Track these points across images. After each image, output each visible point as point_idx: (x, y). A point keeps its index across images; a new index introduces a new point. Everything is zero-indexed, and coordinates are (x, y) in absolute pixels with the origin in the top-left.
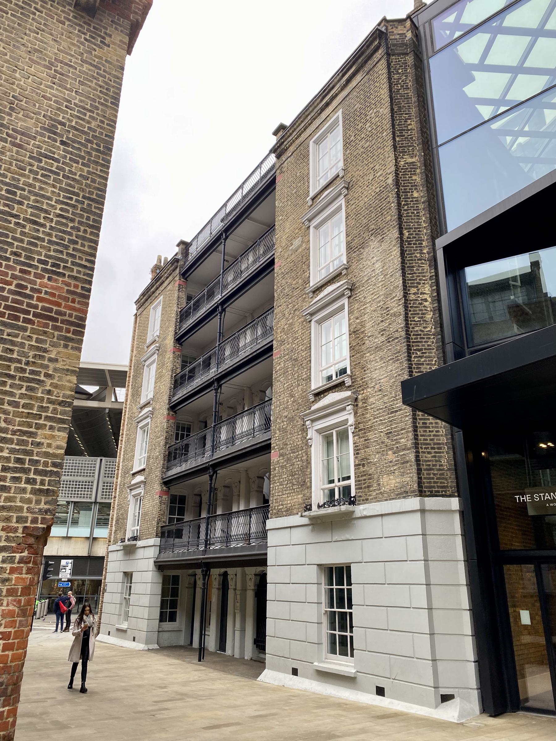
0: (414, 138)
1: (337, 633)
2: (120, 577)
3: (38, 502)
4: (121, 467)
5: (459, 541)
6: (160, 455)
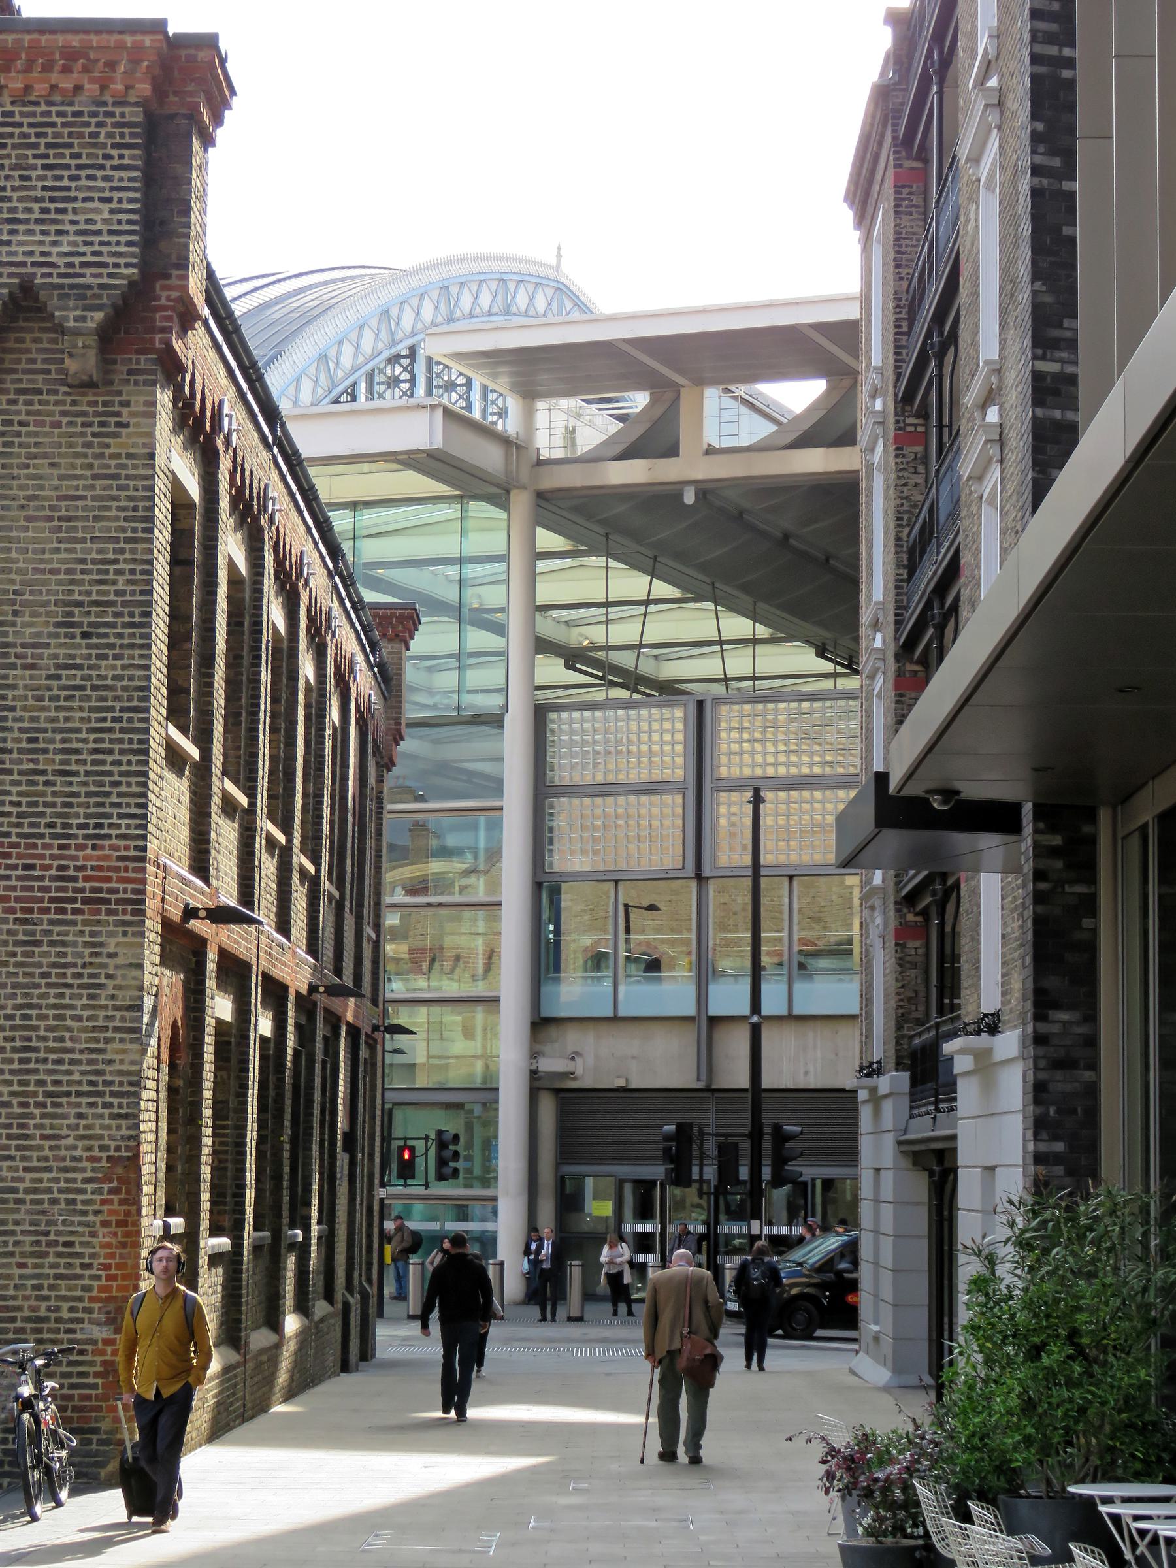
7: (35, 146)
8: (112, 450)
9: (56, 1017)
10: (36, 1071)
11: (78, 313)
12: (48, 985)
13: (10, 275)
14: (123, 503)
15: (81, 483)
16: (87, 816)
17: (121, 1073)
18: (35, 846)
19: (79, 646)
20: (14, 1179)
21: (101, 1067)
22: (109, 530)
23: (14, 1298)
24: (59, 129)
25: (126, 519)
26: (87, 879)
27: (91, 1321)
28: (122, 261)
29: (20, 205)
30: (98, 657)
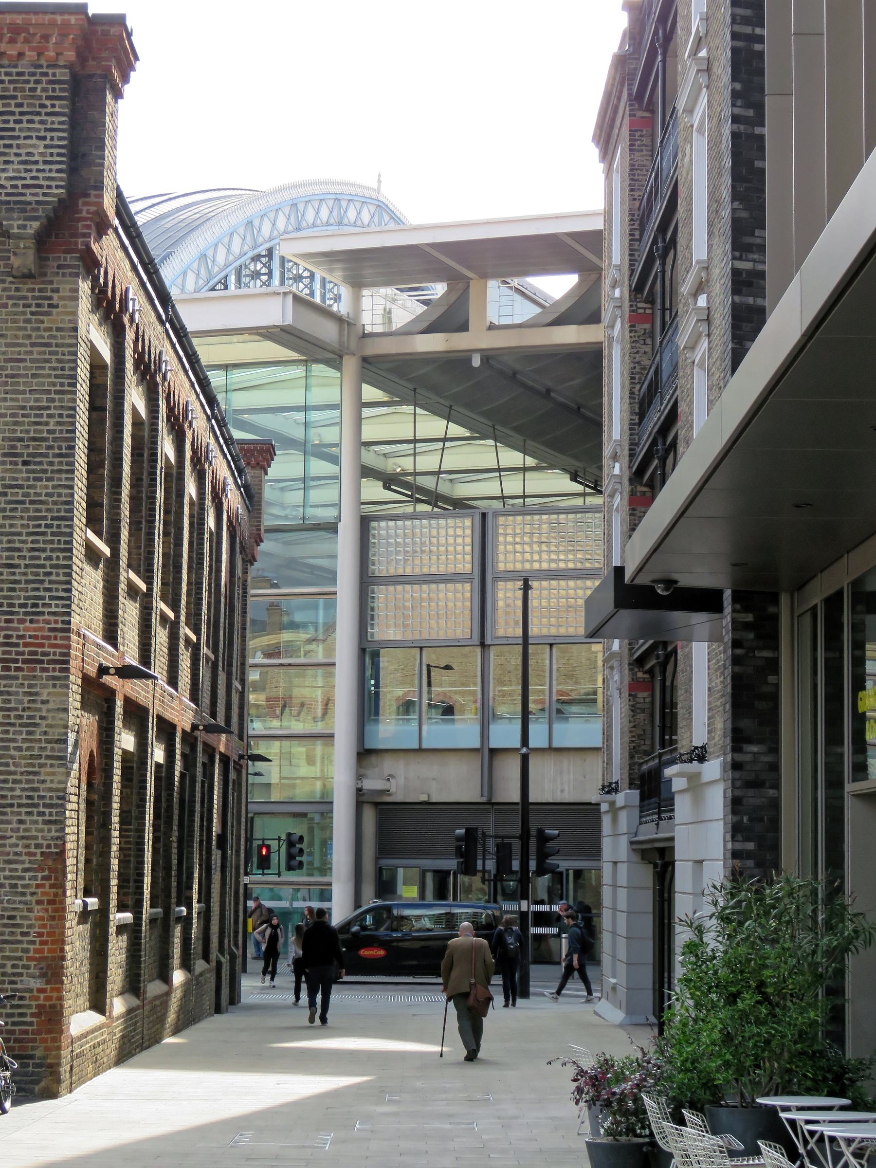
3: (49, 831)
11: (20, 222)
14: (54, 365)
15: (22, 349)
16: (26, 598)
17: (51, 790)
19: (21, 471)
21: (36, 785)
22: (43, 384)
25: (56, 376)
26: (26, 645)
27: (28, 975)
28: (53, 184)
30: (35, 479)
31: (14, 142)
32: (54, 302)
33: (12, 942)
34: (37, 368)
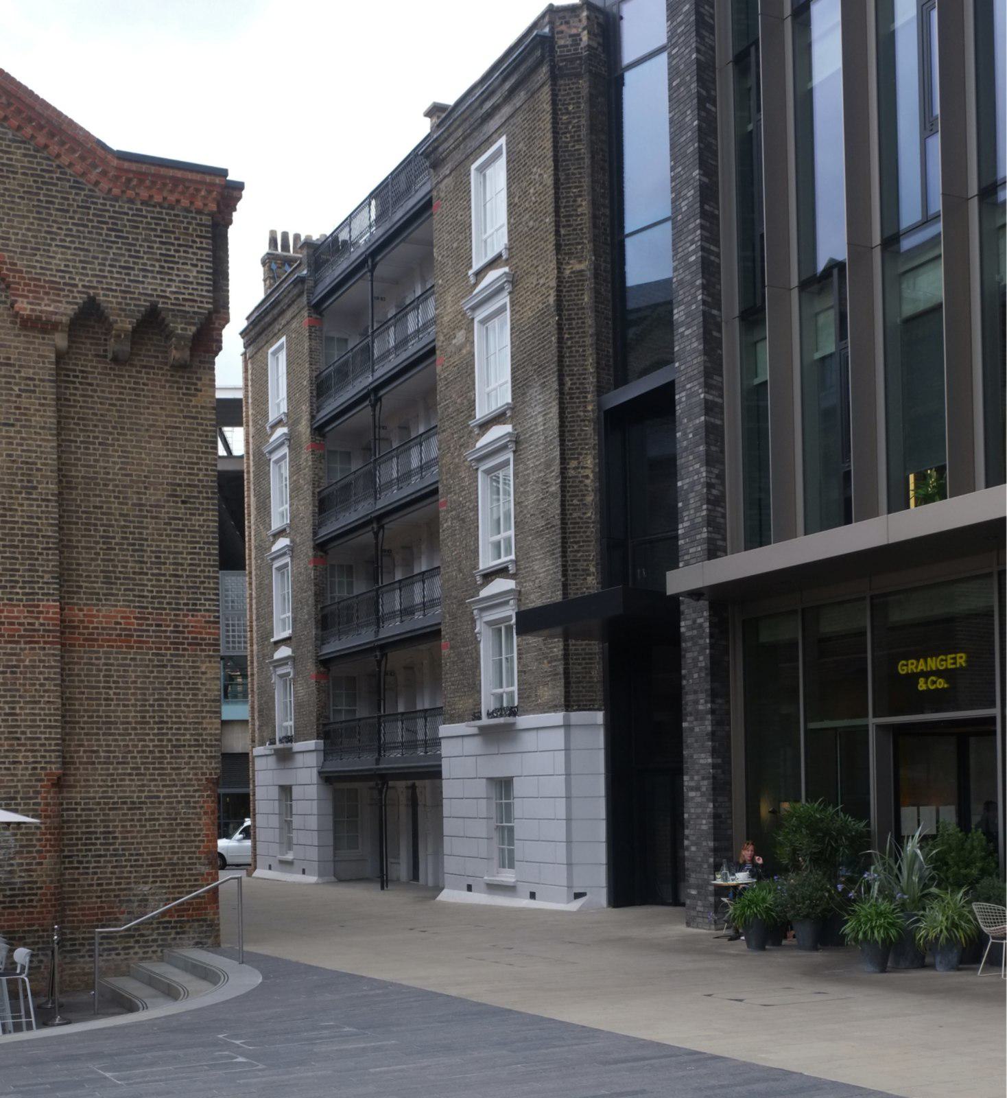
0: (585, 230)
1: (505, 847)
2: (274, 793)
3: (211, 763)
4: (255, 628)
5: (601, 756)
6: (309, 619)
7: (155, 230)
8: (193, 403)
9: (176, 705)
10: (167, 734)
11: (183, 326)
12: (172, 689)
13: (145, 301)
14: (201, 432)
15: (178, 420)
16: (188, 599)
17: (211, 734)
18: (161, 614)
19: (180, 508)
20: (157, 791)
21: (200, 731)
22: (193, 446)
23: (160, 853)
24: (167, 222)
25: (202, 441)
26: (189, 632)
27: (200, 864)
28: (205, 300)
29: (149, 263)
30: (191, 514)
31: (176, 266)
32: (199, 387)
33: (188, 842)
34: (189, 434)
